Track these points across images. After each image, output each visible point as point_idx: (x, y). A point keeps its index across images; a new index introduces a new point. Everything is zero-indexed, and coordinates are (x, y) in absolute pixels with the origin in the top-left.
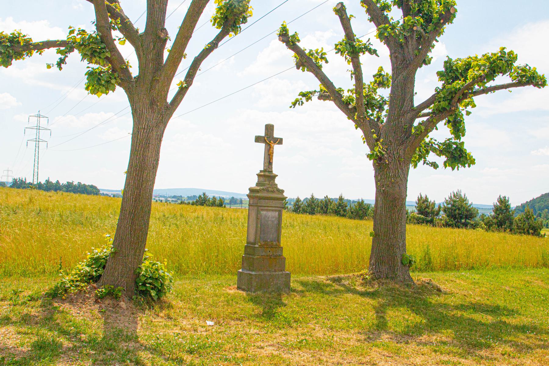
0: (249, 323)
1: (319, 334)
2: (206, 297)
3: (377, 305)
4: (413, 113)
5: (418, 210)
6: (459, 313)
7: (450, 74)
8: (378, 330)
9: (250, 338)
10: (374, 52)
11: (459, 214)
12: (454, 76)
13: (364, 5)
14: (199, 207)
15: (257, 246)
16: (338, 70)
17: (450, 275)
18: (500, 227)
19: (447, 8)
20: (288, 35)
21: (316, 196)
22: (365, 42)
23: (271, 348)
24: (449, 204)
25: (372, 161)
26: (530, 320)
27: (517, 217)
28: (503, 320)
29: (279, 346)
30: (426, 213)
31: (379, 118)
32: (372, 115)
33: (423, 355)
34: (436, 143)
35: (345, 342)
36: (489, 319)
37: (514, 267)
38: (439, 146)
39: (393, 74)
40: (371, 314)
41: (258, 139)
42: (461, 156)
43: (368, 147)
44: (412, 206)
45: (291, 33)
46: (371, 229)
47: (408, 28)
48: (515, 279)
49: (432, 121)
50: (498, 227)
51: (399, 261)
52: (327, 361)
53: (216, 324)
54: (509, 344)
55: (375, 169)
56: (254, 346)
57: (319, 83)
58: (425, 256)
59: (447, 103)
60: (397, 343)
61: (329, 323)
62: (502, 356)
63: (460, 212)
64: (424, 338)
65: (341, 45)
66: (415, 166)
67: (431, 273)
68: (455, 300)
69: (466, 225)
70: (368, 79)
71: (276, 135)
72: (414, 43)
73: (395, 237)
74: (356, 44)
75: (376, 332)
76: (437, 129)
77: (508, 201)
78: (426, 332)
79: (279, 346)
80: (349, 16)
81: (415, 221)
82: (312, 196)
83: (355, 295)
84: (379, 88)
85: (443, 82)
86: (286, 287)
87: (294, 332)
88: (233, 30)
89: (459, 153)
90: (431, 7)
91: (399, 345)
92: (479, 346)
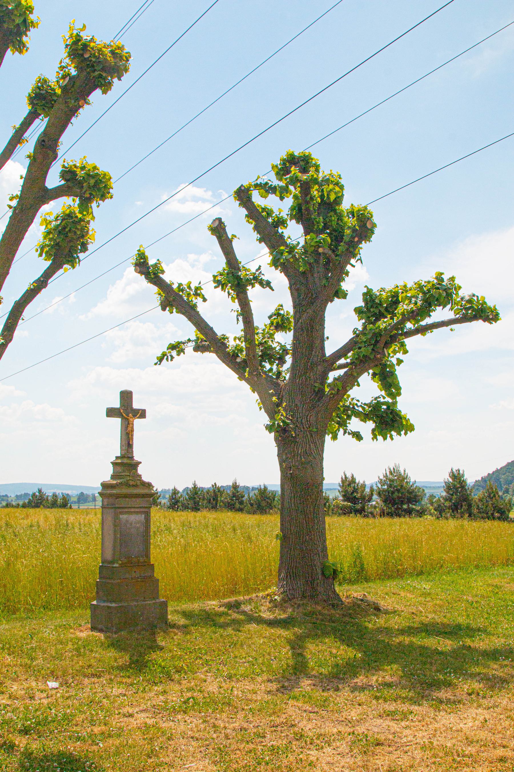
0: (111, 680)
1: (212, 687)
2: (45, 645)
3: (292, 638)
4: (325, 364)
5: (344, 496)
6: (407, 640)
7: (372, 310)
8: (296, 674)
9: (113, 702)
10: (268, 284)
11: (399, 498)
12: (377, 311)
13: (251, 221)
14: (31, 511)
15: (116, 565)
16: (220, 311)
17: (391, 585)
18: (455, 512)
19: (362, 221)
20: (148, 264)
21: (199, 485)
22: (254, 271)
23: (143, 715)
24: (384, 485)
25: (273, 434)
26: (503, 640)
27: (476, 496)
28: (467, 644)
29: (156, 711)
30: (354, 498)
31: (279, 374)
32: (271, 370)
33: (359, 705)
34: (359, 404)
35: (249, 696)
36: (446, 645)
37: (477, 567)
38: (364, 409)
39: (295, 313)
40: (284, 651)
41: (111, 412)
42: (393, 421)
43: (266, 415)
44: (335, 489)
45: (151, 262)
46: (277, 531)
47: (312, 251)
48: (479, 584)
49: (352, 375)
50: (453, 511)
51: (319, 571)
52: (225, 728)
53: (61, 685)
54: (478, 678)
55: (278, 446)
56: (119, 713)
57: (194, 328)
58: (355, 562)
59: (370, 348)
60: (323, 691)
61: (225, 670)
62: (468, 697)
63: (400, 495)
64: (360, 680)
65: (221, 275)
66: (335, 437)
67: (366, 585)
68: (399, 621)
69: (409, 512)
70: (261, 320)
71: (136, 405)
72: (322, 269)
73: (311, 539)
74: (242, 274)
75: (293, 678)
76: (358, 385)
77: (463, 475)
78: (363, 670)
79: (156, 711)
80: (230, 237)
81: (340, 511)
82: (195, 485)
83: (261, 626)
84: (277, 331)
85: (363, 321)
86: (160, 622)
87: (177, 687)
88: (68, 262)
89: (391, 416)
90: (342, 220)
91: (325, 694)
92: (436, 685)
